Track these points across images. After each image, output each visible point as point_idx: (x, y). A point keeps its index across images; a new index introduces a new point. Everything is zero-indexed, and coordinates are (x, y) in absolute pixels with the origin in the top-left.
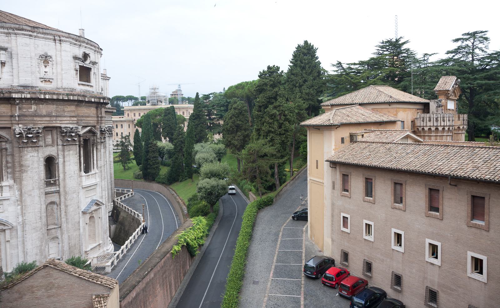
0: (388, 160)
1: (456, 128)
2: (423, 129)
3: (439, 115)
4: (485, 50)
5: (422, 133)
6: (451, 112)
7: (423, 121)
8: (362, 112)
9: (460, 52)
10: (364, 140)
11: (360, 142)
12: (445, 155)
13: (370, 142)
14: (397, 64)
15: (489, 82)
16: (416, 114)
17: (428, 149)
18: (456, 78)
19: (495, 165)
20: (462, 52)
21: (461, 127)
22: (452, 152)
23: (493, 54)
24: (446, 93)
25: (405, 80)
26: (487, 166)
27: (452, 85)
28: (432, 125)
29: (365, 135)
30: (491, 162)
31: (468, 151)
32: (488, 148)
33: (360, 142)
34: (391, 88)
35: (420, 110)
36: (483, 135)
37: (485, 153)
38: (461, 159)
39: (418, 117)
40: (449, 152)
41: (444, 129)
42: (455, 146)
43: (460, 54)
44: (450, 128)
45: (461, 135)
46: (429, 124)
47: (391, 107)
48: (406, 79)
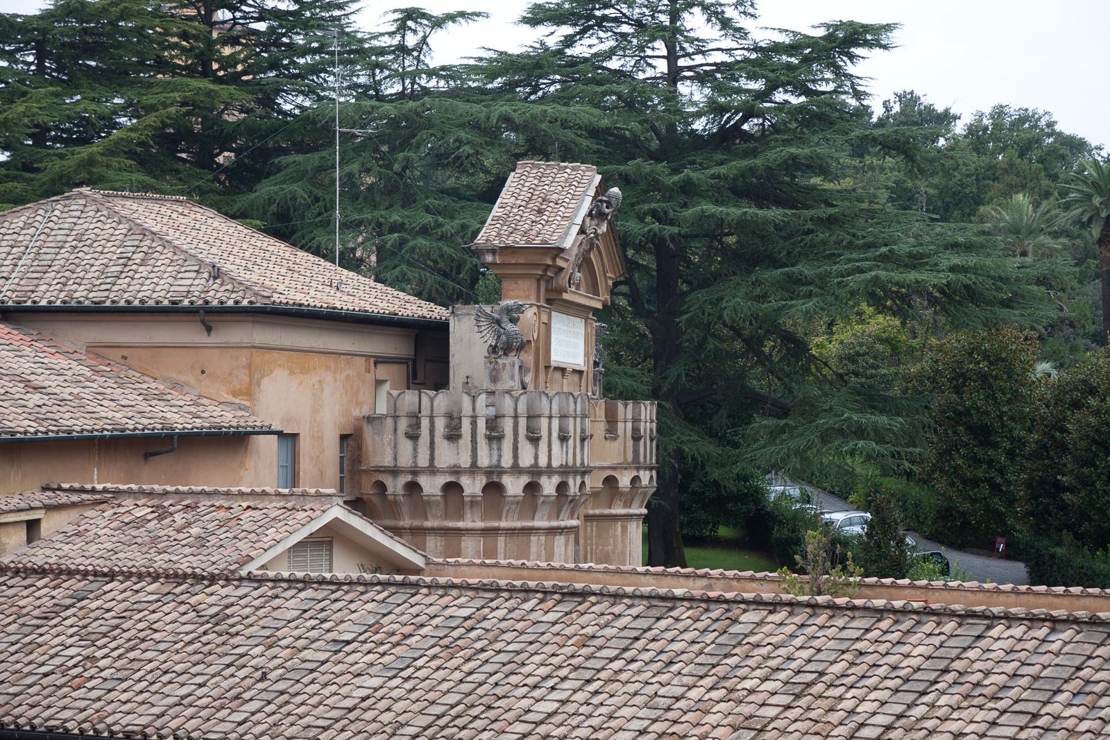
0: (215, 693)
1: (594, 482)
2: (413, 487)
3: (508, 403)
4: (743, 22)
5: (405, 510)
6: (568, 384)
7: (413, 437)
8: (24, 366)
9: (605, 18)
10: (40, 556)
11: (17, 572)
12: (568, 651)
13: (85, 574)
14: (231, 61)
15: (760, 212)
16: (365, 393)
17: (465, 612)
18: (599, 178)
19: (852, 712)
20: (616, 20)
21: (624, 481)
22: (608, 632)
23: (777, 48)
24: (541, 264)
25: (279, 169)
26: (813, 715)
27: (579, 220)
28: (465, 461)
29: (50, 524)
30: (830, 693)
31: (700, 625)
32: (808, 605)
33: (17, 572)
34: (211, 213)
35: (395, 368)
36: (723, 531)
37: (793, 636)
38: (663, 678)
39: (382, 409)
40: (589, 630)
41: (532, 488)
42: (625, 596)
43: (602, 34)
44: (571, 482)
45: (624, 529)
46: (447, 455)
47: (214, 339)
48: (285, 160)
